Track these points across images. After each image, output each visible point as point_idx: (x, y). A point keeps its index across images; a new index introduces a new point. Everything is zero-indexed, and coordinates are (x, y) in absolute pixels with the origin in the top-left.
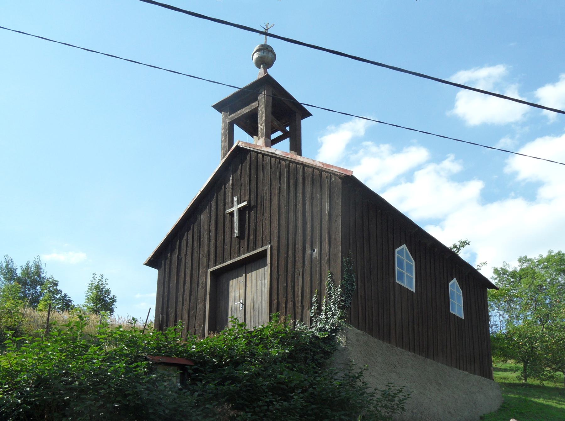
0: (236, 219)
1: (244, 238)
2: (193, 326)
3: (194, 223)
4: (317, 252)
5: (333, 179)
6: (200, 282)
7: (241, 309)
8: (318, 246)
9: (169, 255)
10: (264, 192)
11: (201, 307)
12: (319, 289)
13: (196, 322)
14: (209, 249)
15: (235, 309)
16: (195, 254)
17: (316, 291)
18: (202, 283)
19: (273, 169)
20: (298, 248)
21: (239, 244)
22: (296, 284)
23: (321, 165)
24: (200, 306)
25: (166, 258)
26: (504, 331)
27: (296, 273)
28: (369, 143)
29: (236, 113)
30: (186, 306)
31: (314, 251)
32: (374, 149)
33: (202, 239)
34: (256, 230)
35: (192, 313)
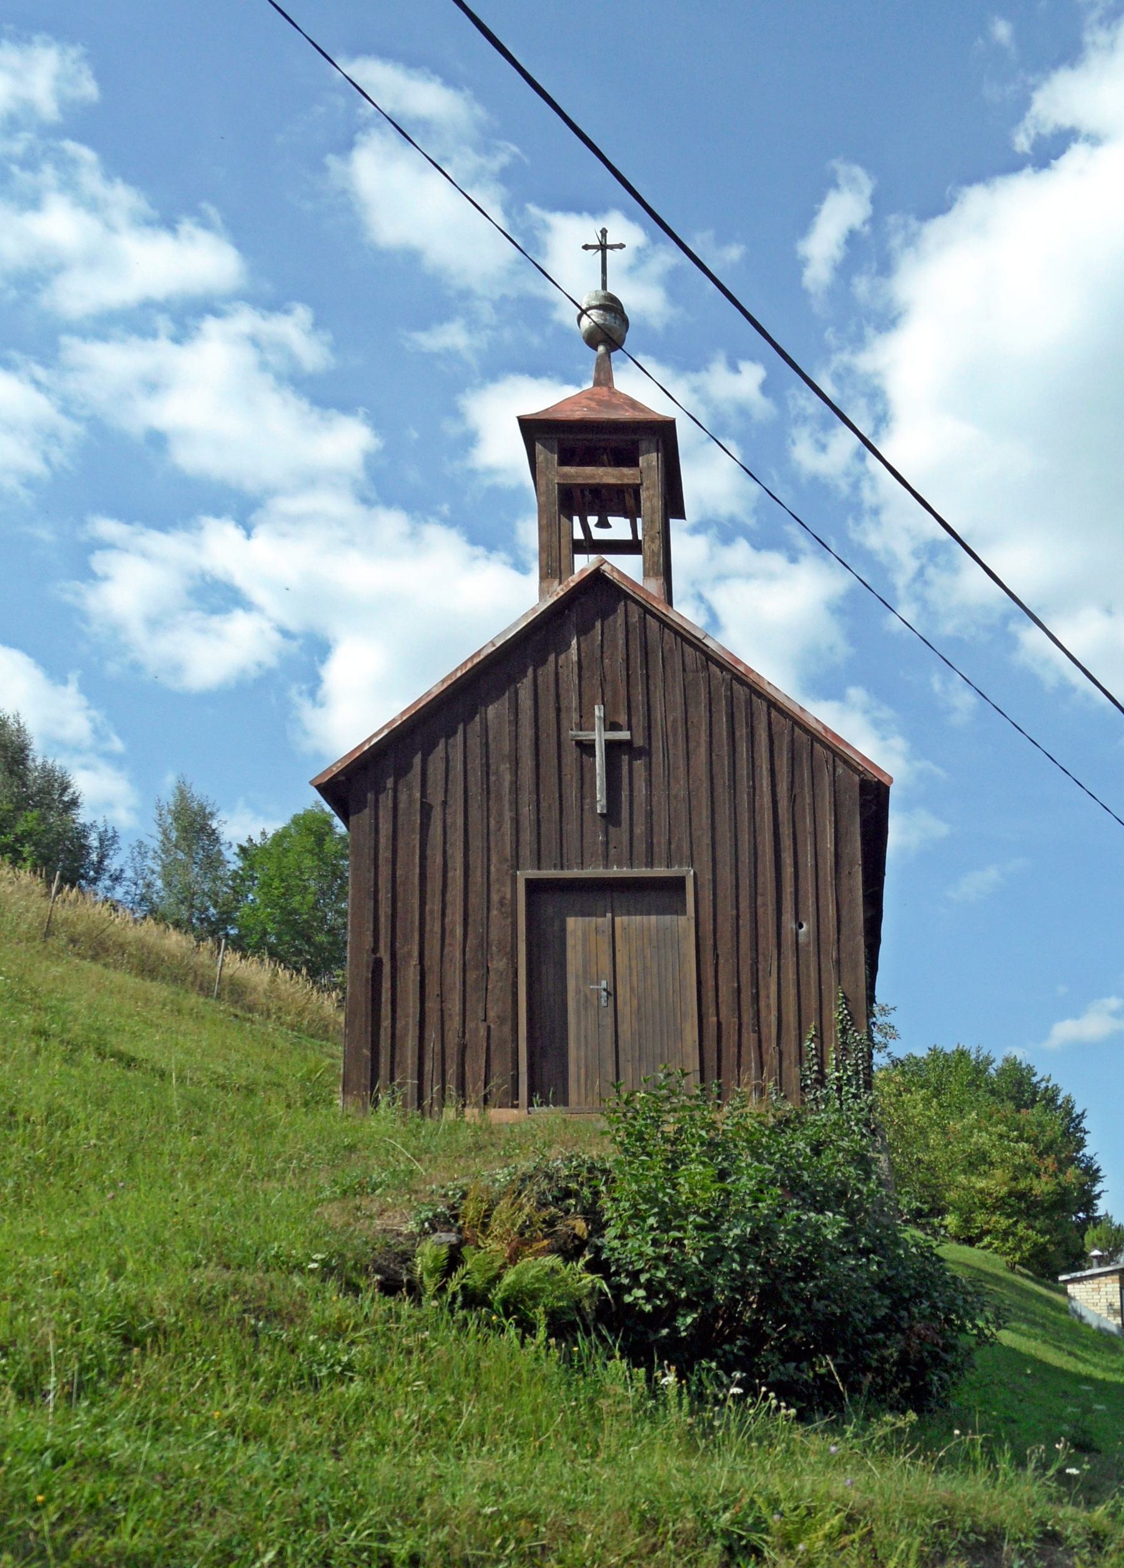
0: (601, 767)
1: (617, 823)
2: (481, 1015)
3: (468, 719)
4: (809, 932)
5: (840, 771)
6: (495, 898)
7: (604, 1003)
8: (812, 918)
9: (390, 783)
10: (669, 724)
11: (501, 969)
12: (818, 1023)
13: (489, 1006)
14: (517, 814)
15: (586, 1000)
16: (475, 813)
17: (812, 1026)
18: (502, 903)
19: (690, 676)
20: (764, 904)
21: (607, 834)
22: (762, 993)
23: (820, 729)
24: (499, 964)
25: (379, 790)
26: (339, 1050)
27: (760, 967)
28: (87, 154)
29: (580, 469)
30: (455, 952)
31: (801, 926)
32: (91, 180)
33: (492, 778)
34: (650, 814)
35: (472, 976)
